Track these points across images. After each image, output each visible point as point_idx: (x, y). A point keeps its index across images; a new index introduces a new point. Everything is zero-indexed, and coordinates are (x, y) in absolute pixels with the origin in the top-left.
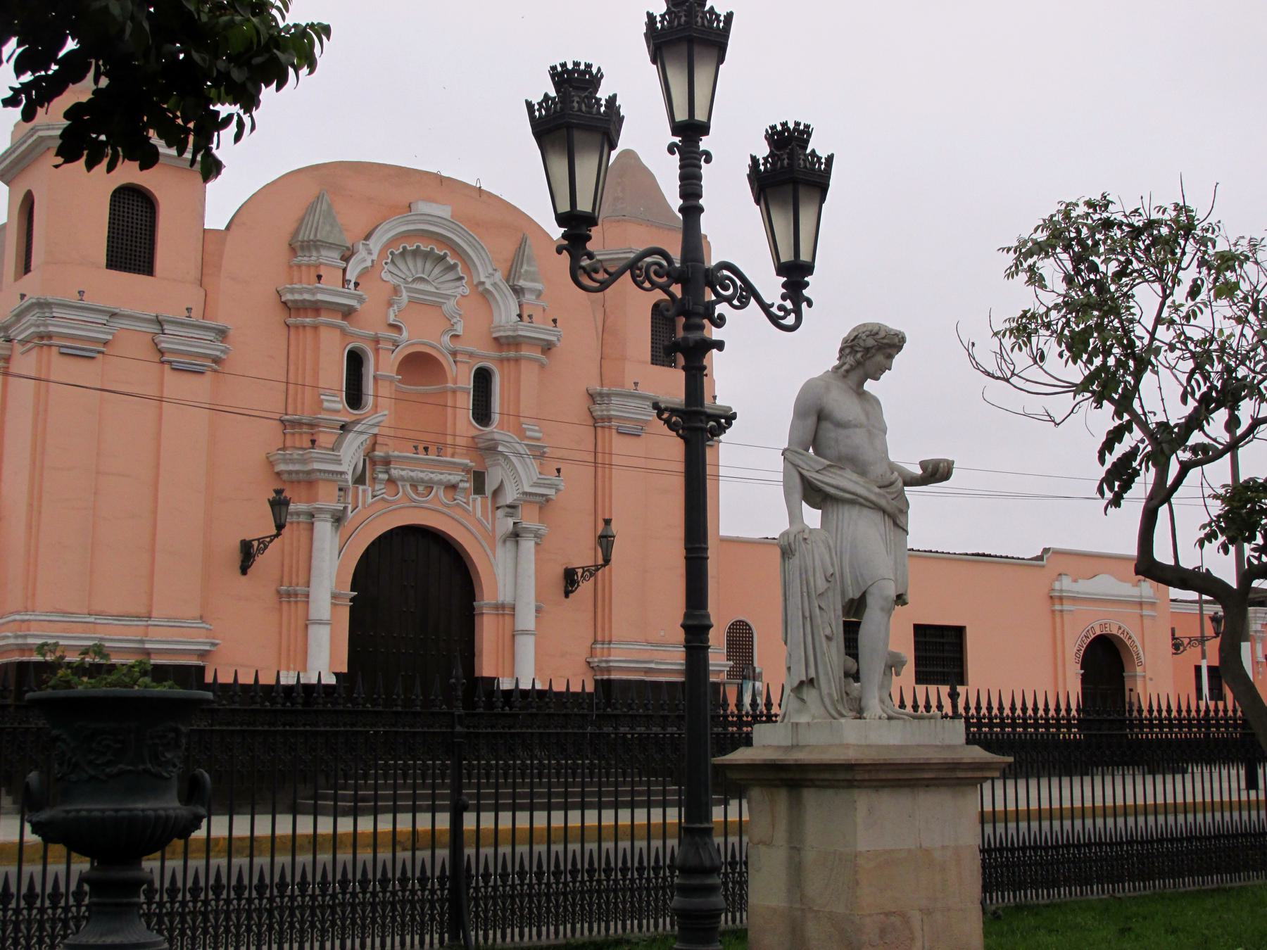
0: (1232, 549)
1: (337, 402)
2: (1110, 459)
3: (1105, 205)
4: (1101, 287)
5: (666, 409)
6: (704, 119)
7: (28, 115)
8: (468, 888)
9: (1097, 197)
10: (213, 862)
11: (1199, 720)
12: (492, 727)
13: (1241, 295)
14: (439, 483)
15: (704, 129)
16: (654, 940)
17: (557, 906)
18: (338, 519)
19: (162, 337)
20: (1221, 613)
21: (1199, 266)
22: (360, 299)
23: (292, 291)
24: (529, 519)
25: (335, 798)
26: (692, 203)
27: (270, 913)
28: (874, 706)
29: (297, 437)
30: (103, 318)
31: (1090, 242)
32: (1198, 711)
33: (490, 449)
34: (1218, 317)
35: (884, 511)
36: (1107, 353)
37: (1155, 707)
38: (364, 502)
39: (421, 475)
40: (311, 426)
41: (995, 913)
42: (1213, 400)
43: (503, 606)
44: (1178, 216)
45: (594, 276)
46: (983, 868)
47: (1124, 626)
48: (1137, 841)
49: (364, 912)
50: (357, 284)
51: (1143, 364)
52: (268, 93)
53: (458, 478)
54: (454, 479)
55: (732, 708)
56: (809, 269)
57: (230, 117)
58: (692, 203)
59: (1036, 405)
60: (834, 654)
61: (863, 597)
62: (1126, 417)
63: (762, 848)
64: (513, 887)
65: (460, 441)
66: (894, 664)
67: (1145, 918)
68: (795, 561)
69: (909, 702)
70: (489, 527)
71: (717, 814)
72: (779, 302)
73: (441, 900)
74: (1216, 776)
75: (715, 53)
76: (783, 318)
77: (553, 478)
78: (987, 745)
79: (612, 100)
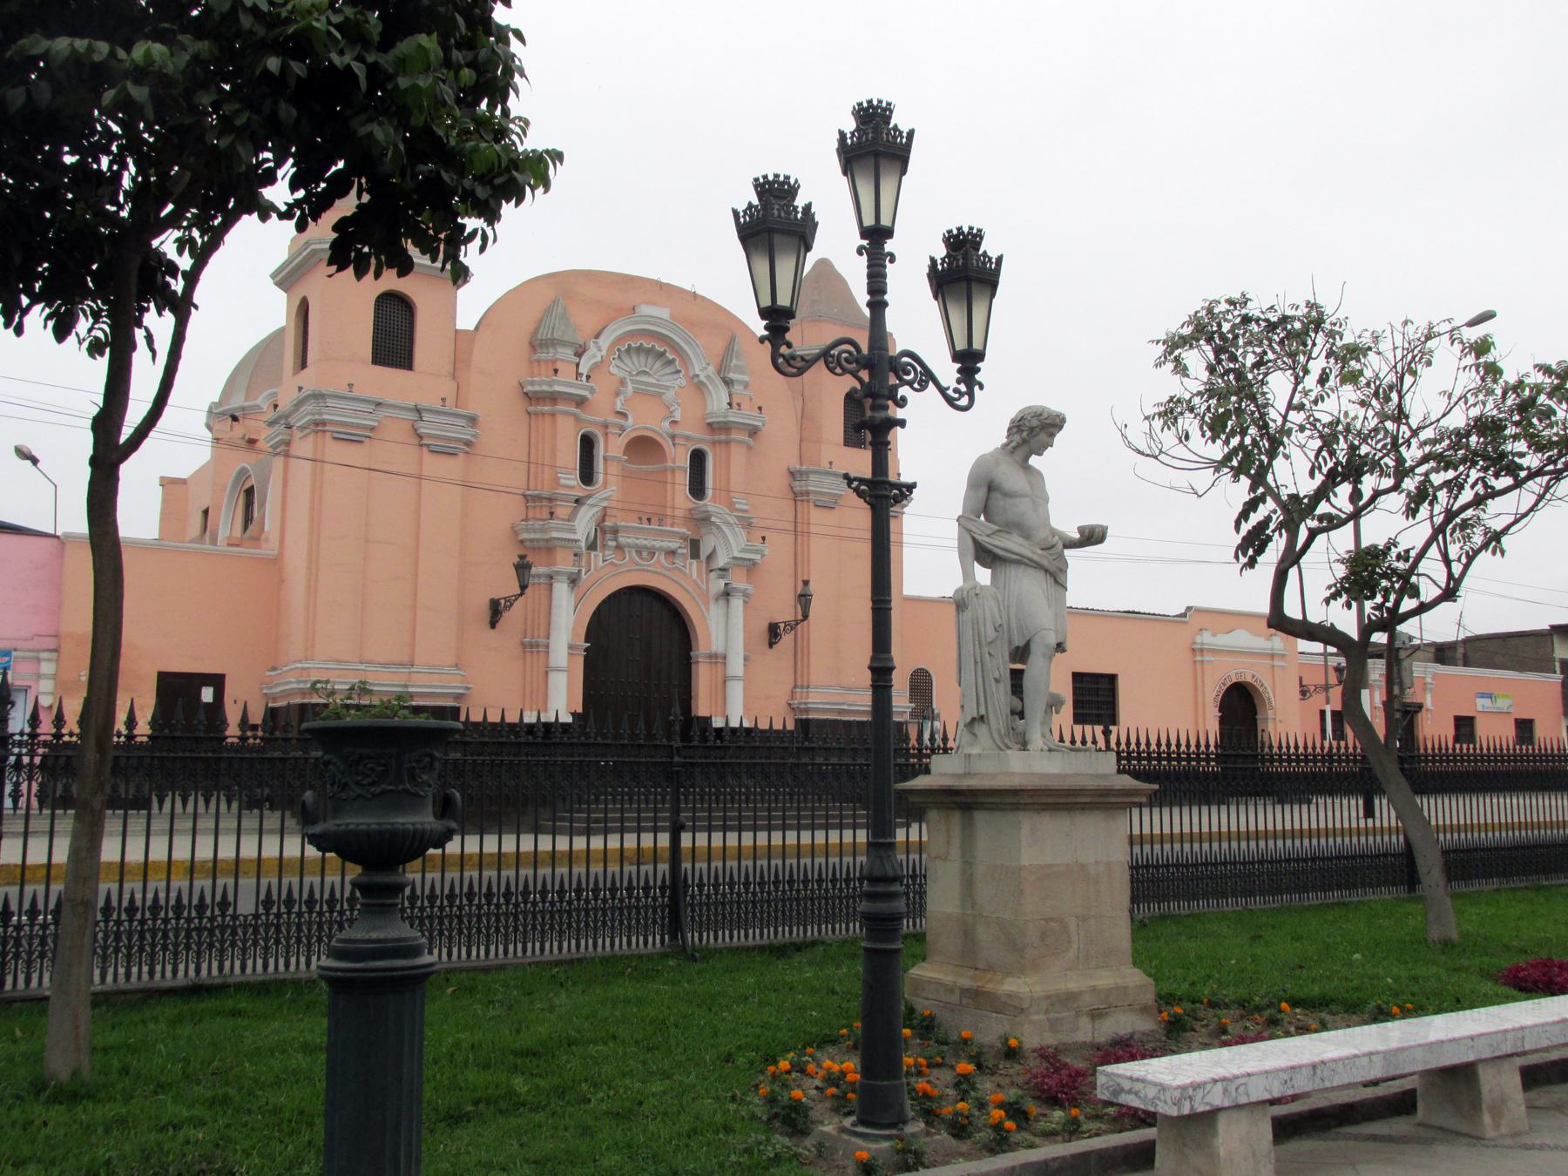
0: (1354, 604)
1: (572, 479)
2: (1246, 527)
3: (1245, 301)
4: (1240, 375)
5: (855, 479)
6: (889, 224)
7: (301, 227)
8: (686, 896)
9: (1236, 295)
10: (467, 874)
11: (1323, 756)
12: (706, 758)
13: (1365, 381)
14: (661, 549)
15: (888, 233)
16: (845, 942)
17: (762, 912)
18: (574, 581)
19: (420, 424)
20: (1344, 664)
21: (1327, 357)
22: (592, 391)
23: (532, 383)
24: (739, 582)
25: (571, 821)
26: (878, 298)
27: (569, 913)
28: (1036, 740)
29: (538, 510)
30: (370, 408)
31: (1230, 336)
32: (1322, 748)
33: (704, 520)
34: (1344, 401)
35: (1046, 571)
36: (1244, 433)
37: (1284, 744)
38: (596, 566)
39: (645, 542)
40: (550, 500)
41: (1141, 921)
42: (1339, 474)
43: (716, 656)
44: (1309, 312)
45: (792, 362)
46: (1132, 882)
47: (1257, 675)
48: (1267, 861)
49: (543, 919)
50: (588, 377)
51: (1275, 443)
52: (507, 209)
53: (677, 545)
54: (673, 545)
55: (913, 742)
56: (980, 356)
57: (475, 232)
58: (878, 298)
59: (1182, 479)
60: (1001, 695)
61: (1028, 644)
62: (1261, 490)
63: (938, 862)
64: (724, 895)
65: (678, 513)
66: (1054, 704)
67: (1273, 927)
68: (968, 615)
69: (1067, 738)
70: (704, 587)
71: (900, 835)
72: (954, 385)
73: (663, 906)
74: (1468, 802)
75: (899, 165)
76: (958, 399)
77: (758, 544)
78: (1136, 775)
79: (808, 208)
